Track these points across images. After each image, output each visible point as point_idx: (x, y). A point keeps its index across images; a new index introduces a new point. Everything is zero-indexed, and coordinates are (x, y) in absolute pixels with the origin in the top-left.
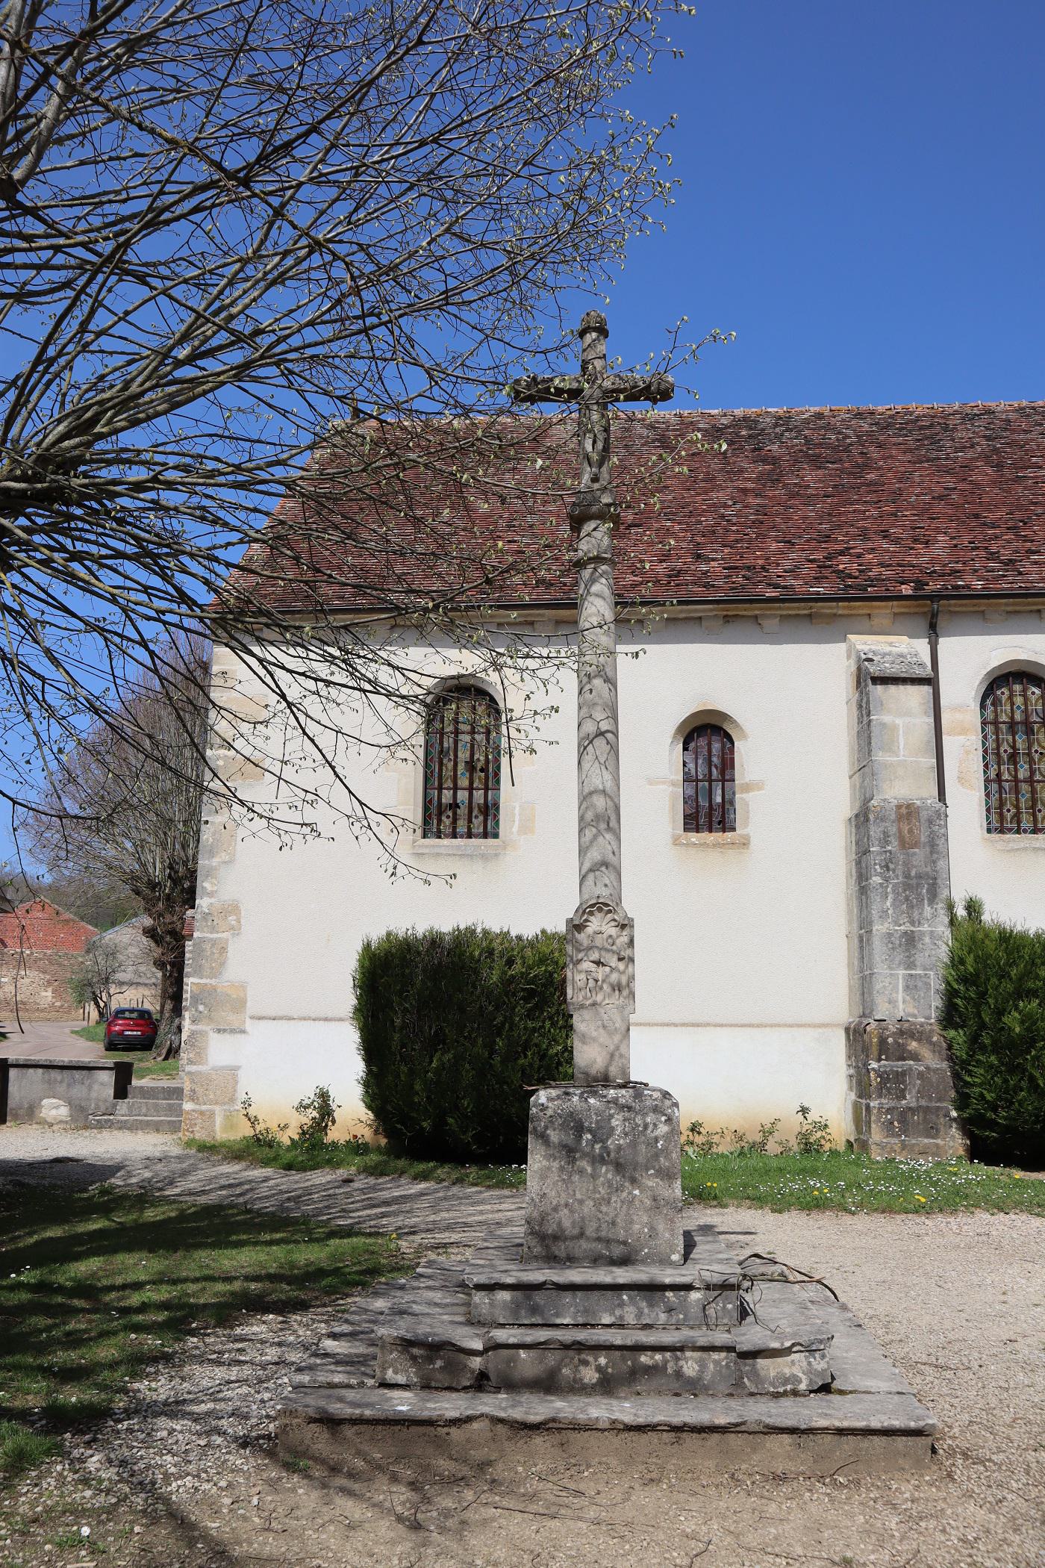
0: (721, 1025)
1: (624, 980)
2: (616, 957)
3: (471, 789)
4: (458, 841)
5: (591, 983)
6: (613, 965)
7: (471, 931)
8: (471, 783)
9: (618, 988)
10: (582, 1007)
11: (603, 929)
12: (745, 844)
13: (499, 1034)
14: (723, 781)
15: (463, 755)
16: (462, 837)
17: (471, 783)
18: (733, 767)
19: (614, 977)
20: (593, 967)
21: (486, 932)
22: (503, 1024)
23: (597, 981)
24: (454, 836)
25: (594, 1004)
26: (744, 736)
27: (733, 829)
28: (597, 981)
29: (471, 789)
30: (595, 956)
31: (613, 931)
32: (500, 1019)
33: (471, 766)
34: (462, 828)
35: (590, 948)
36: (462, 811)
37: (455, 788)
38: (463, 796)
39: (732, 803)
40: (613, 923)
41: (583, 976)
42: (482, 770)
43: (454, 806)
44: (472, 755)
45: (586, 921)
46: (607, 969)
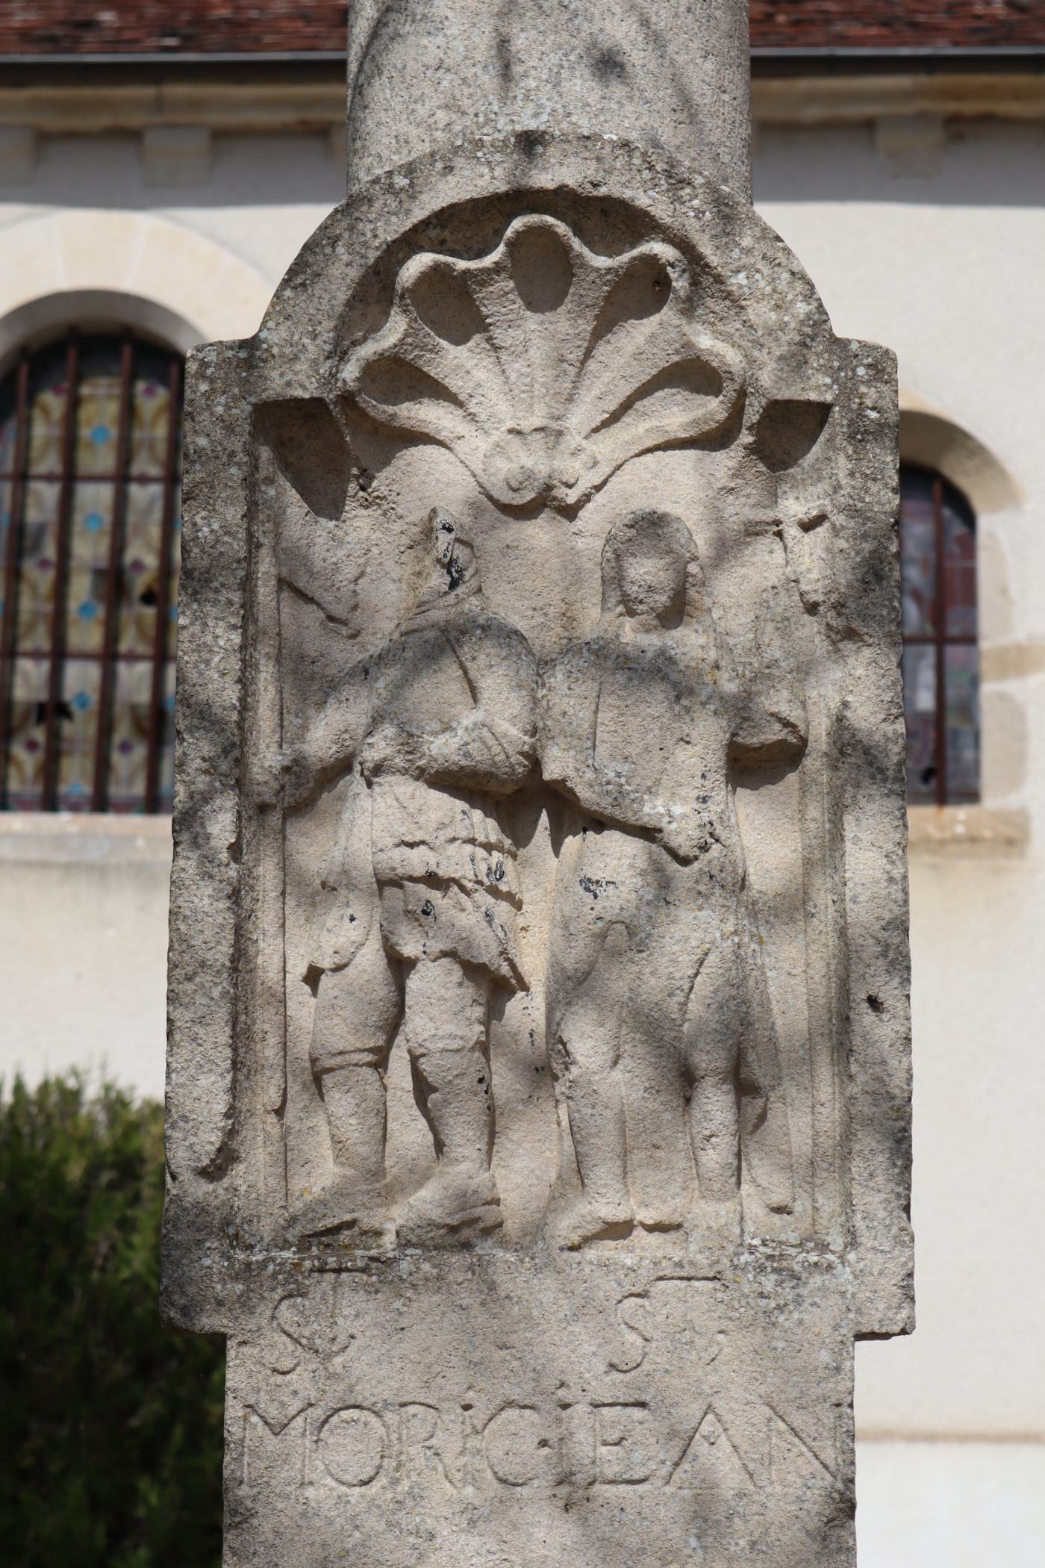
0: (931, 1437)
1: (791, 981)
2: (704, 743)
3: (109, 657)
4: (64, 822)
5: (439, 1012)
6: (677, 813)
7: (64, 1098)
8: (112, 635)
9: (721, 1063)
10: (328, 1245)
11: (574, 467)
12: (1012, 840)
13: (149, 1463)
14: (941, 641)
15: (89, 548)
16: (75, 808)
17: (112, 635)
18: (970, 597)
19: (691, 946)
20: (451, 834)
21: (115, 1103)
22: (163, 1428)
23: (495, 985)
24: (50, 803)
25: (467, 1230)
26: (1009, 494)
27: (971, 796)
28: (495, 985)
29: (109, 657)
30: (485, 715)
31: (685, 489)
32: (152, 1408)
33: (113, 581)
34: (76, 777)
35: (440, 642)
36: (80, 729)
37: (59, 654)
38: (81, 678)
39: (969, 710)
40: (678, 412)
41: (347, 935)
42: (148, 598)
43: (53, 710)
44: (118, 548)
45: (403, 376)
46: (616, 857)
